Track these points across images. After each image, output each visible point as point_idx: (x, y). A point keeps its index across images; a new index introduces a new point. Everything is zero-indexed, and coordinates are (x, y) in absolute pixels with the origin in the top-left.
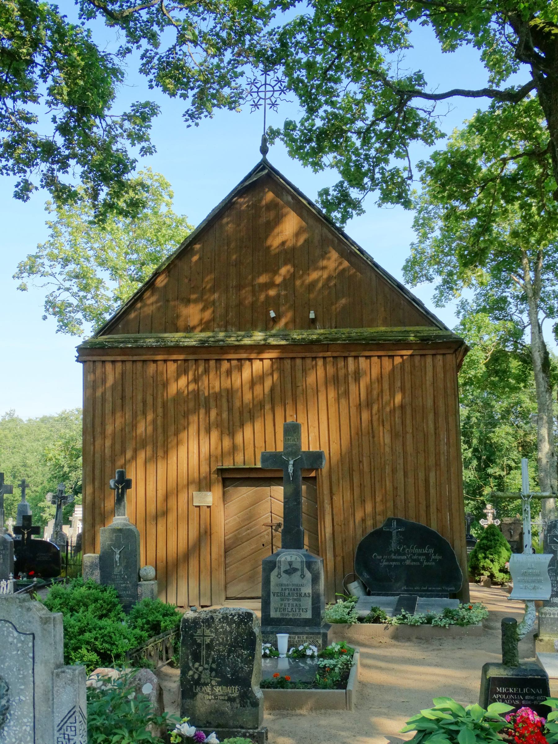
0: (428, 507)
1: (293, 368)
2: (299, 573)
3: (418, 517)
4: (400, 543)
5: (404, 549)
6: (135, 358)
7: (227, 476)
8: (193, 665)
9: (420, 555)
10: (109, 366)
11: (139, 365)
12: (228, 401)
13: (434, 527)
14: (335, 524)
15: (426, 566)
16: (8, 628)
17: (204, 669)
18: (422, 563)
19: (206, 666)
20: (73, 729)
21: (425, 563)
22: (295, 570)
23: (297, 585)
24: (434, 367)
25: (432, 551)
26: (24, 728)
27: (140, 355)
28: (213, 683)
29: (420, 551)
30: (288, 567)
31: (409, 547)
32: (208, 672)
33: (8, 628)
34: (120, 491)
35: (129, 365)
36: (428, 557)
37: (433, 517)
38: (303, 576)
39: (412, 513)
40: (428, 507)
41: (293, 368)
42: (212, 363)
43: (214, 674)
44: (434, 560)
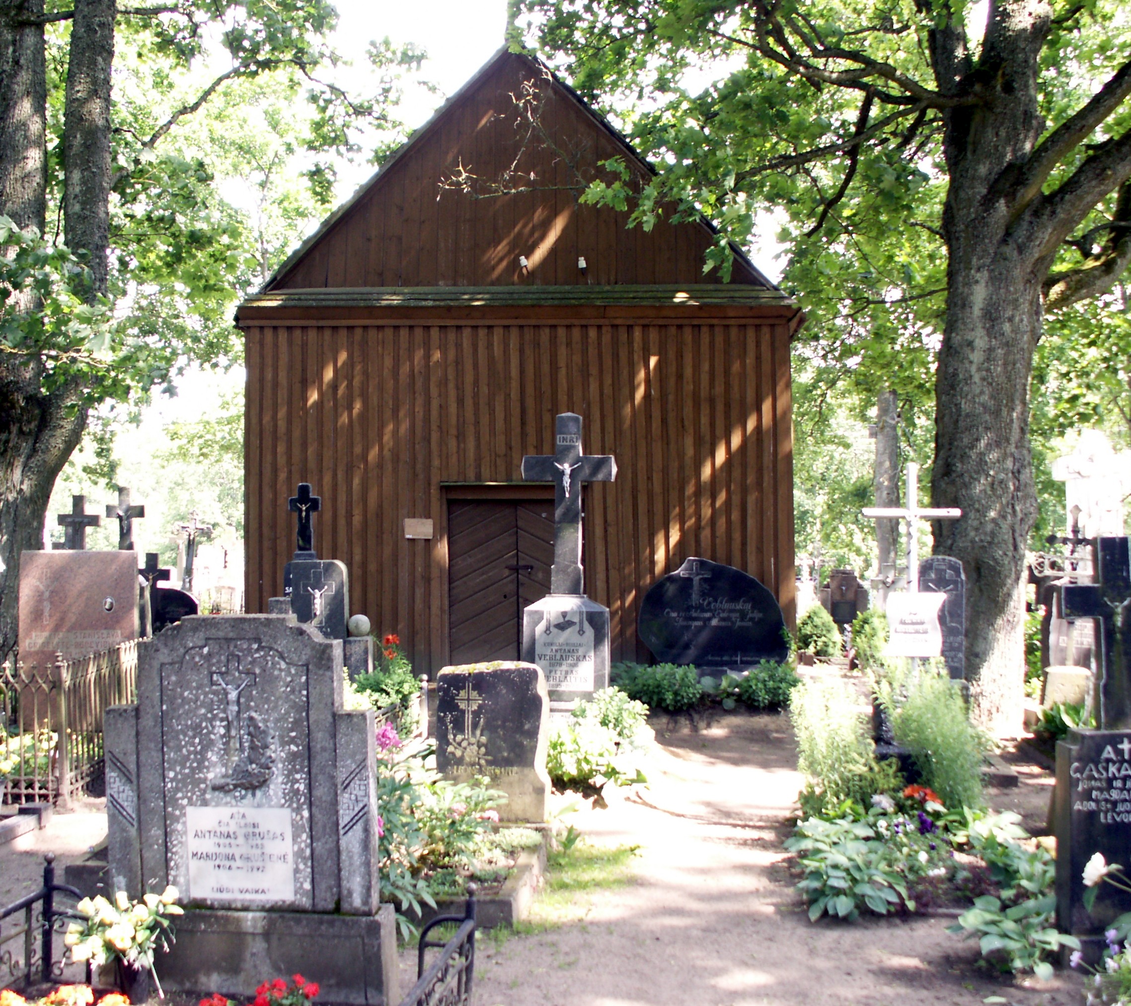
0: (744, 544)
1: (553, 340)
2: (577, 627)
3: (729, 561)
4: (703, 594)
5: (709, 603)
6: (321, 323)
7: (454, 496)
8: (454, 740)
9: (731, 611)
10: (283, 336)
11: (328, 333)
12: (457, 388)
13: (752, 573)
14: (610, 567)
15: (739, 627)
16: (273, 657)
17: (469, 744)
18: (734, 623)
19: (473, 740)
20: (363, 788)
21: (738, 623)
22: (570, 624)
23: (574, 645)
24: (758, 344)
25: (748, 606)
26: (296, 786)
27: (333, 318)
28: (483, 762)
29: (732, 606)
30: (562, 620)
31: (716, 601)
32: (475, 747)
33: (273, 657)
34: (304, 514)
35: (312, 335)
36: (743, 615)
37: (752, 559)
38: (581, 632)
39: (721, 552)
40: (744, 544)
41: (553, 340)
42: (435, 333)
43: (483, 750)
44: (751, 619)
